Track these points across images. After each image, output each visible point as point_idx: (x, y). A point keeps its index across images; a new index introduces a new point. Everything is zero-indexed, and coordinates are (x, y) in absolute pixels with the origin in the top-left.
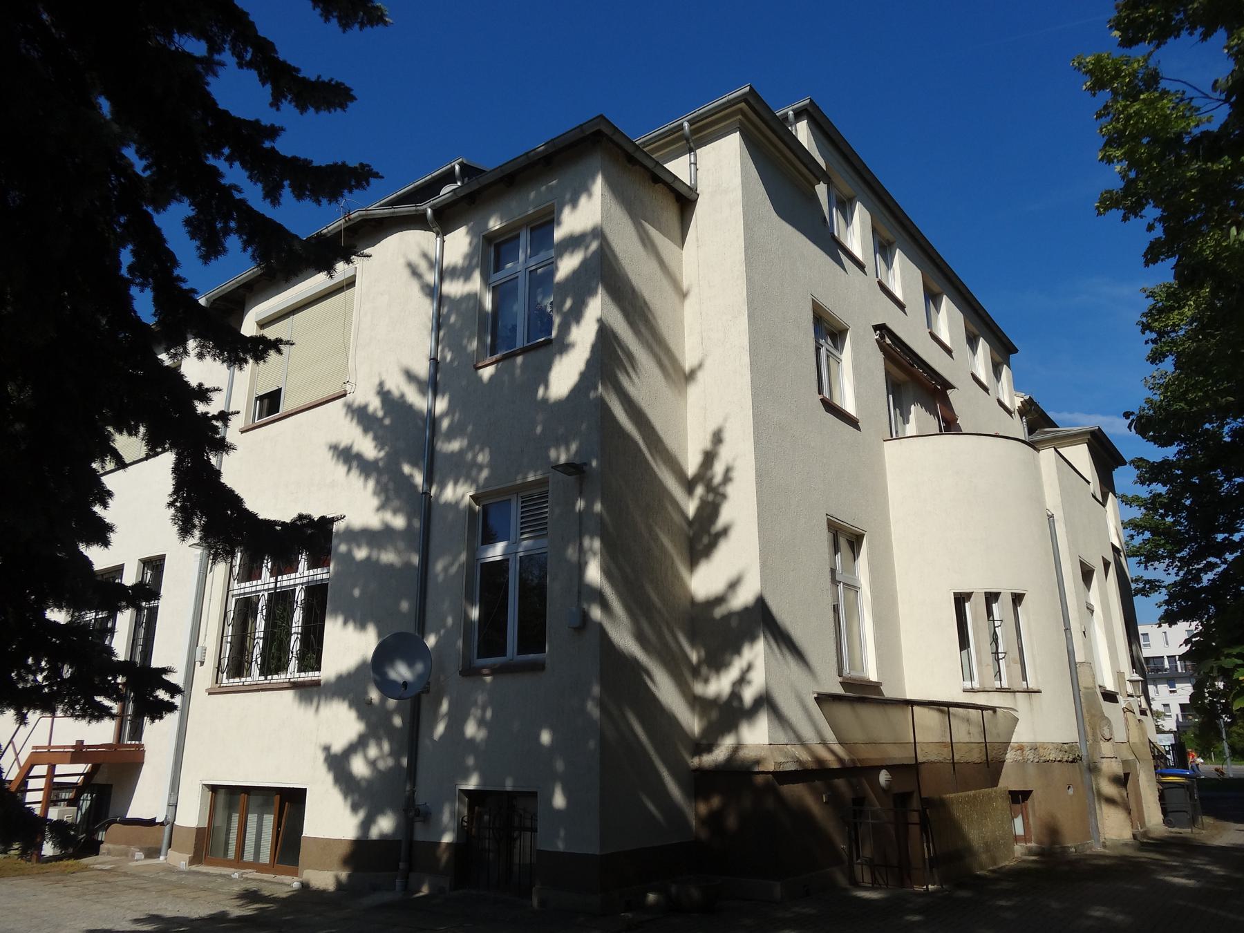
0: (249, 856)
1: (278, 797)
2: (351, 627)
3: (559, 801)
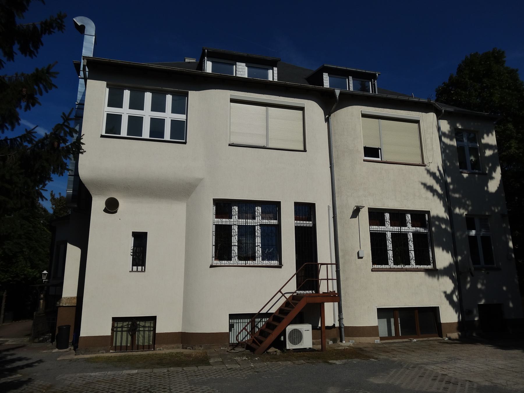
0: (393, 334)
1: (417, 311)
2: (445, 252)
3: (511, 305)
